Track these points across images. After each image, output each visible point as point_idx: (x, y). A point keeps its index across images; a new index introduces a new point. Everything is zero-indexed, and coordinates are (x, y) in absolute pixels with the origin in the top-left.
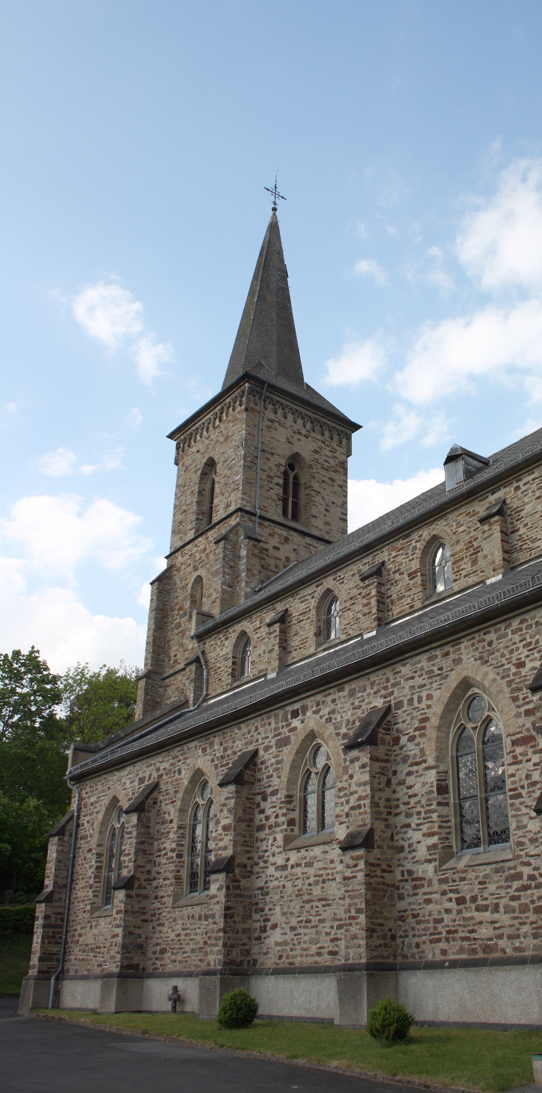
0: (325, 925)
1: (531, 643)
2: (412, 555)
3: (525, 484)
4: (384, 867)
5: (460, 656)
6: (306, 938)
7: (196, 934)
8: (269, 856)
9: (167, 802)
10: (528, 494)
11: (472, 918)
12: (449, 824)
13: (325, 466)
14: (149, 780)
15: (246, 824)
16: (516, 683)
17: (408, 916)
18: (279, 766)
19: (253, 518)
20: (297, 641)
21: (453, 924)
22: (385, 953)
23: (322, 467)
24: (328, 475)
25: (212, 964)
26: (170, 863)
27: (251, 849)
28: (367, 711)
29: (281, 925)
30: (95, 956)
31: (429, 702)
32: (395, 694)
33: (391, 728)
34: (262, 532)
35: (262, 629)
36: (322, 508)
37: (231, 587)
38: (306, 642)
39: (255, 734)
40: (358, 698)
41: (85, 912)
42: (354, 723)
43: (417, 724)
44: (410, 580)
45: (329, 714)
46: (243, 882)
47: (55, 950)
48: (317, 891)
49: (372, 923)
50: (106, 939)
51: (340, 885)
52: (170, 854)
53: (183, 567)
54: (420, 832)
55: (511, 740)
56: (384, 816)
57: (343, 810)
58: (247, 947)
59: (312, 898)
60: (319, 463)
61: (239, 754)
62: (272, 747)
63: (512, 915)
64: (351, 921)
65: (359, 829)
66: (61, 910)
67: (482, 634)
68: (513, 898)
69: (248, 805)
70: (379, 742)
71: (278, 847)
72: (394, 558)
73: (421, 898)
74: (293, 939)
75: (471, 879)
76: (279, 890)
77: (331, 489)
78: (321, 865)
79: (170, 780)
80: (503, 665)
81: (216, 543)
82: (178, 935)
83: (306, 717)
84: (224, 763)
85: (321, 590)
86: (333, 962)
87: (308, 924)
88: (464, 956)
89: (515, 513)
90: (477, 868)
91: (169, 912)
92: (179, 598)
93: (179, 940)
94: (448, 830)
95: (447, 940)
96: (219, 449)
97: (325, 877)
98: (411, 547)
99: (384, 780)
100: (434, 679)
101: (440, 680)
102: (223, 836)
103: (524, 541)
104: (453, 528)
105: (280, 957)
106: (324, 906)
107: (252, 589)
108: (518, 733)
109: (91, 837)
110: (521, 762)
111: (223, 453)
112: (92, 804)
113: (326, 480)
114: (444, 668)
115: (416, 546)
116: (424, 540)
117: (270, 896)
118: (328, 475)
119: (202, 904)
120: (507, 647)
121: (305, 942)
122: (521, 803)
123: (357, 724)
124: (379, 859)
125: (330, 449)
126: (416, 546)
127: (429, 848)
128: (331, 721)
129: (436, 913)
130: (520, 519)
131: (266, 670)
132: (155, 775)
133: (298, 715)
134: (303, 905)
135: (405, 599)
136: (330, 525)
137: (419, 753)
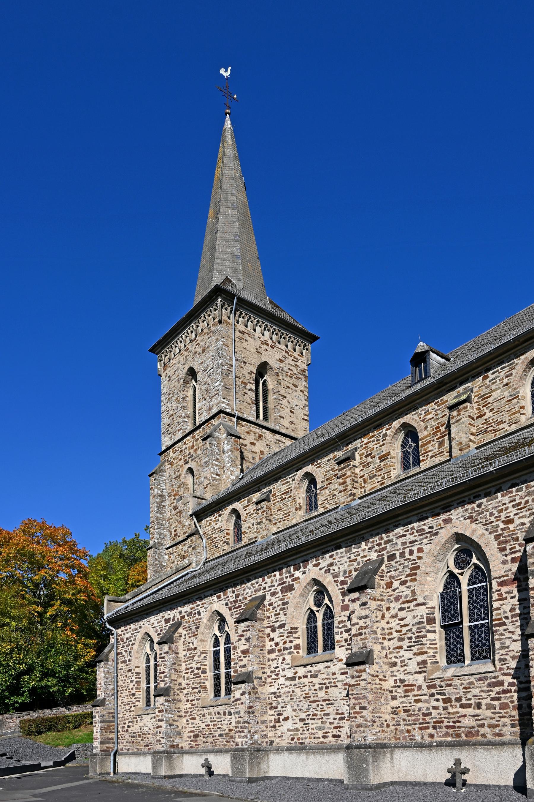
0: (329, 717)
1: (521, 503)
2: (382, 441)
3: (493, 373)
4: (381, 677)
5: (450, 516)
6: (314, 726)
7: (222, 725)
8: (279, 671)
9: (190, 635)
10: (496, 382)
11: (457, 713)
12: (436, 646)
13: (289, 374)
14: (173, 620)
15: (260, 649)
16: (504, 537)
17: (400, 711)
18: (285, 606)
19: (232, 418)
20: (281, 515)
21: (439, 716)
22: (383, 737)
23: (287, 375)
24: (291, 381)
25: (240, 744)
26: (196, 677)
27: (265, 666)
28: (363, 563)
29: (292, 717)
30: (142, 740)
31: (420, 554)
32: (388, 549)
33: (385, 575)
34: (241, 430)
35: (250, 507)
36: (288, 410)
37: (219, 475)
38: (289, 515)
39: (263, 584)
40: (354, 553)
41: (130, 711)
42: (350, 572)
43: (409, 571)
44: (380, 462)
45: (328, 566)
46: (260, 689)
47: (110, 737)
48: (321, 694)
49: (373, 716)
50: (150, 729)
51: (341, 690)
52: (196, 671)
53: (175, 462)
54: (411, 652)
55: (497, 582)
56: (380, 641)
57: (342, 637)
58: (265, 733)
59: (318, 699)
60: (284, 371)
61: (249, 599)
62: (278, 593)
63: (493, 711)
64: (356, 715)
65: (360, 650)
66: (112, 711)
67: (472, 498)
68: (493, 699)
69: (261, 635)
70: (376, 586)
71: (287, 664)
72: (366, 444)
73: (411, 699)
74: (302, 727)
75: (456, 685)
76: (289, 694)
77: (295, 394)
78: (325, 676)
79: (191, 620)
80: (493, 522)
81: (203, 440)
82: (208, 725)
83: (307, 569)
84: (237, 605)
85: (300, 474)
86: (337, 742)
87: (315, 717)
88: (449, 739)
89: (482, 400)
90: (462, 677)
91: (198, 710)
92: (174, 486)
93: (209, 729)
94: (435, 650)
95: (434, 728)
96: (199, 359)
97: (328, 685)
98: (382, 435)
99: (380, 614)
100: (424, 536)
101: (431, 536)
102: (242, 658)
103: (490, 424)
104: (422, 416)
105: (292, 739)
106: (327, 704)
107: (236, 477)
108: (504, 576)
109: (129, 661)
110: (506, 598)
111: (202, 363)
112: (127, 639)
113: (290, 385)
114: (435, 526)
115: (386, 433)
116: (394, 428)
117: (282, 698)
118: (291, 381)
119: (225, 705)
120: (496, 507)
121: (313, 729)
122: (505, 630)
123: (354, 574)
124: (377, 672)
125: (292, 358)
126: (386, 433)
127: (419, 664)
128: (329, 572)
129: (425, 709)
130: (487, 405)
131: (256, 538)
132: (178, 616)
133: (300, 568)
134: (310, 704)
135: (376, 478)
136: (294, 424)
137: (410, 594)
